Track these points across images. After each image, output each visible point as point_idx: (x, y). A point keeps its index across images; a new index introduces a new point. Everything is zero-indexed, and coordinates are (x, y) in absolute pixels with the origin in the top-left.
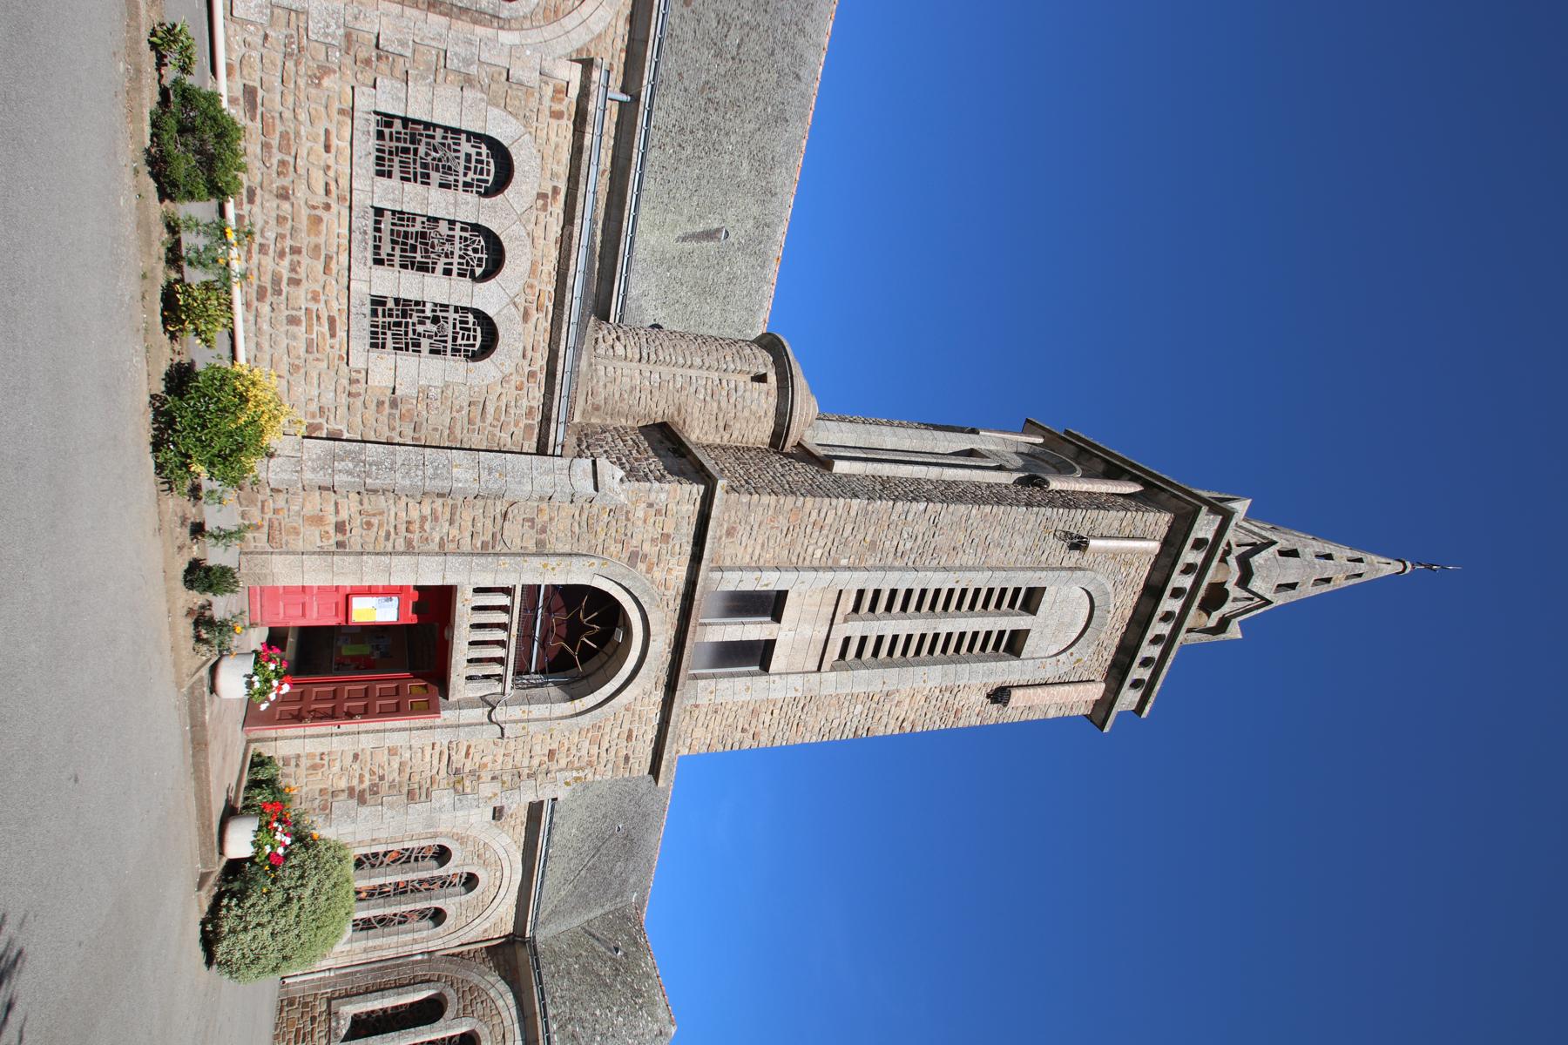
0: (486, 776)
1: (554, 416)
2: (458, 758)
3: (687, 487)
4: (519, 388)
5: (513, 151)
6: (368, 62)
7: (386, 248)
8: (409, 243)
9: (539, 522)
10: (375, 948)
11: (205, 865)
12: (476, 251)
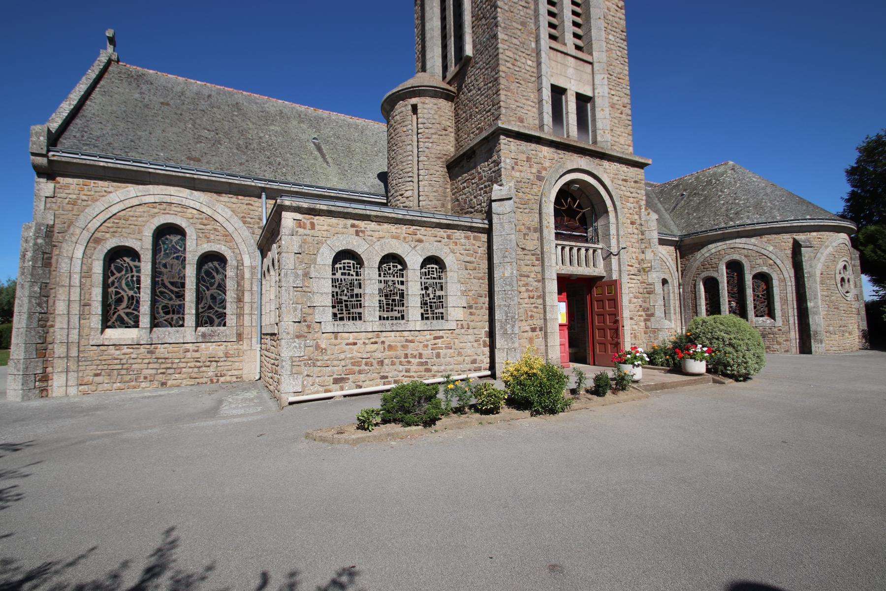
0: (642, 256)
1: (469, 224)
2: (633, 270)
3: (502, 146)
4: (456, 244)
5: (337, 250)
6: (309, 327)
7: (396, 314)
8: (392, 302)
9: (525, 231)
10: (675, 310)
11: (709, 381)
12: (390, 269)
